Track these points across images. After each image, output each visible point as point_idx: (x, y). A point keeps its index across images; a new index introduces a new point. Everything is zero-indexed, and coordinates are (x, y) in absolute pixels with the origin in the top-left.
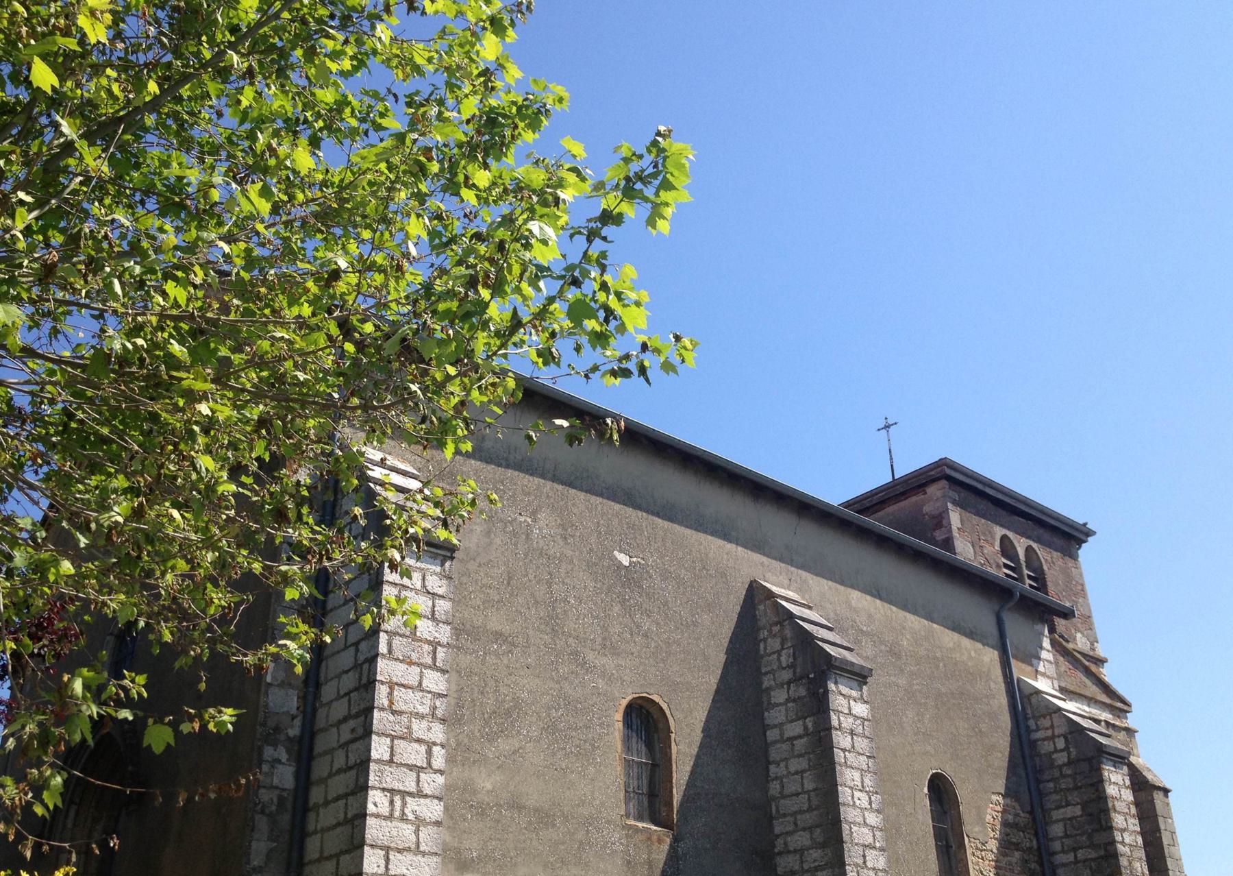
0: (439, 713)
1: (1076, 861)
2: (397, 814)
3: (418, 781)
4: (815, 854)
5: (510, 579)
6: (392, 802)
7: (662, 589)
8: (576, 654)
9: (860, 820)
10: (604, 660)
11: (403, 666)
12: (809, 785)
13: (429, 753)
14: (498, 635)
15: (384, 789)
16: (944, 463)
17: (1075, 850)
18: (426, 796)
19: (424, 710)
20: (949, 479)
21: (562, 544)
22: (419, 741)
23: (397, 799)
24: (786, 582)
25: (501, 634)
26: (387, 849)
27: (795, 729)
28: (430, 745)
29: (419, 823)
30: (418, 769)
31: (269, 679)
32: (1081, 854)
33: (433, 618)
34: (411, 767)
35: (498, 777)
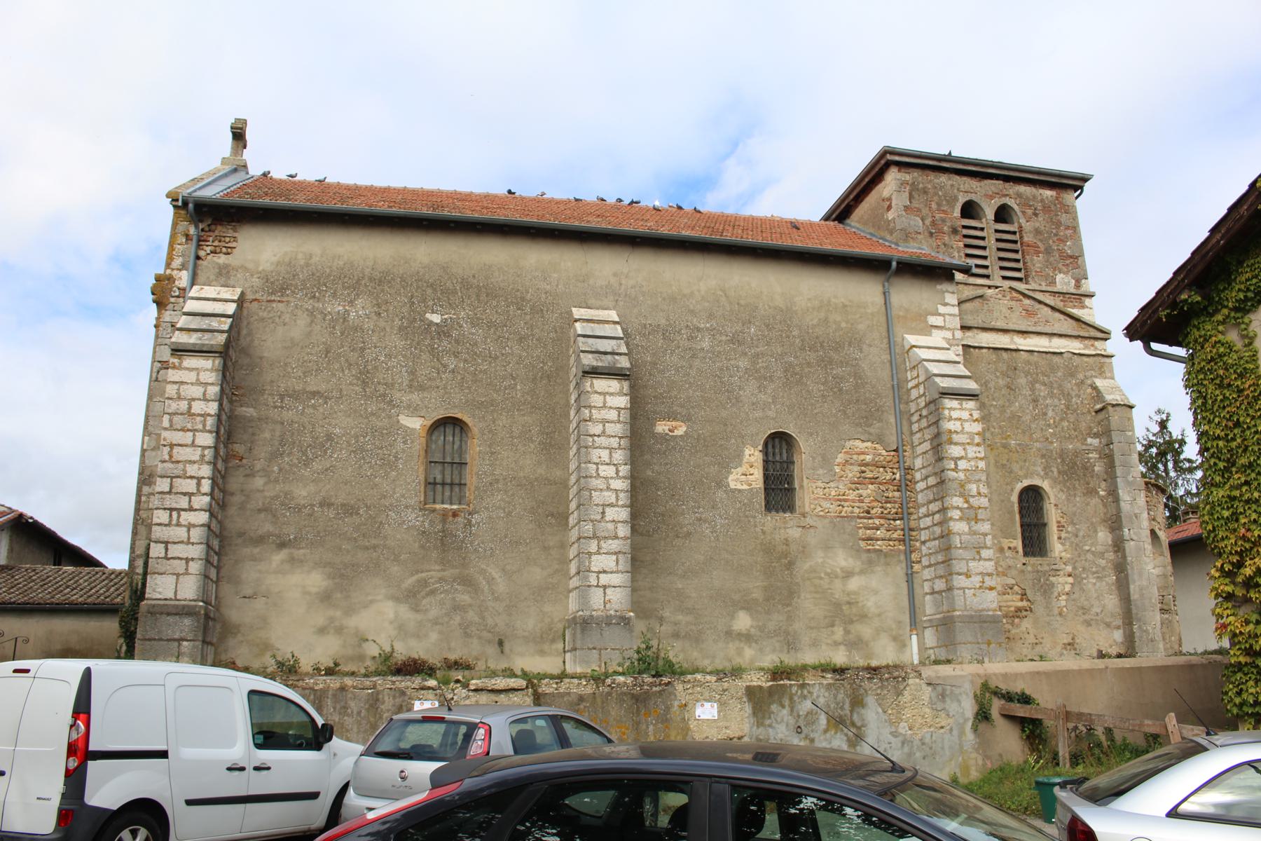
0: (207, 459)
2: (174, 522)
5: (328, 352)
13: (199, 484)
14: (315, 394)
16: (886, 152)
17: (926, 478)
19: (197, 458)
22: (191, 477)
23: (175, 514)
24: (611, 304)
25: (318, 392)
26: (166, 543)
28: (199, 479)
29: (190, 526)
30: (190, 495)
34: (185, 494)
35: (312, 488)
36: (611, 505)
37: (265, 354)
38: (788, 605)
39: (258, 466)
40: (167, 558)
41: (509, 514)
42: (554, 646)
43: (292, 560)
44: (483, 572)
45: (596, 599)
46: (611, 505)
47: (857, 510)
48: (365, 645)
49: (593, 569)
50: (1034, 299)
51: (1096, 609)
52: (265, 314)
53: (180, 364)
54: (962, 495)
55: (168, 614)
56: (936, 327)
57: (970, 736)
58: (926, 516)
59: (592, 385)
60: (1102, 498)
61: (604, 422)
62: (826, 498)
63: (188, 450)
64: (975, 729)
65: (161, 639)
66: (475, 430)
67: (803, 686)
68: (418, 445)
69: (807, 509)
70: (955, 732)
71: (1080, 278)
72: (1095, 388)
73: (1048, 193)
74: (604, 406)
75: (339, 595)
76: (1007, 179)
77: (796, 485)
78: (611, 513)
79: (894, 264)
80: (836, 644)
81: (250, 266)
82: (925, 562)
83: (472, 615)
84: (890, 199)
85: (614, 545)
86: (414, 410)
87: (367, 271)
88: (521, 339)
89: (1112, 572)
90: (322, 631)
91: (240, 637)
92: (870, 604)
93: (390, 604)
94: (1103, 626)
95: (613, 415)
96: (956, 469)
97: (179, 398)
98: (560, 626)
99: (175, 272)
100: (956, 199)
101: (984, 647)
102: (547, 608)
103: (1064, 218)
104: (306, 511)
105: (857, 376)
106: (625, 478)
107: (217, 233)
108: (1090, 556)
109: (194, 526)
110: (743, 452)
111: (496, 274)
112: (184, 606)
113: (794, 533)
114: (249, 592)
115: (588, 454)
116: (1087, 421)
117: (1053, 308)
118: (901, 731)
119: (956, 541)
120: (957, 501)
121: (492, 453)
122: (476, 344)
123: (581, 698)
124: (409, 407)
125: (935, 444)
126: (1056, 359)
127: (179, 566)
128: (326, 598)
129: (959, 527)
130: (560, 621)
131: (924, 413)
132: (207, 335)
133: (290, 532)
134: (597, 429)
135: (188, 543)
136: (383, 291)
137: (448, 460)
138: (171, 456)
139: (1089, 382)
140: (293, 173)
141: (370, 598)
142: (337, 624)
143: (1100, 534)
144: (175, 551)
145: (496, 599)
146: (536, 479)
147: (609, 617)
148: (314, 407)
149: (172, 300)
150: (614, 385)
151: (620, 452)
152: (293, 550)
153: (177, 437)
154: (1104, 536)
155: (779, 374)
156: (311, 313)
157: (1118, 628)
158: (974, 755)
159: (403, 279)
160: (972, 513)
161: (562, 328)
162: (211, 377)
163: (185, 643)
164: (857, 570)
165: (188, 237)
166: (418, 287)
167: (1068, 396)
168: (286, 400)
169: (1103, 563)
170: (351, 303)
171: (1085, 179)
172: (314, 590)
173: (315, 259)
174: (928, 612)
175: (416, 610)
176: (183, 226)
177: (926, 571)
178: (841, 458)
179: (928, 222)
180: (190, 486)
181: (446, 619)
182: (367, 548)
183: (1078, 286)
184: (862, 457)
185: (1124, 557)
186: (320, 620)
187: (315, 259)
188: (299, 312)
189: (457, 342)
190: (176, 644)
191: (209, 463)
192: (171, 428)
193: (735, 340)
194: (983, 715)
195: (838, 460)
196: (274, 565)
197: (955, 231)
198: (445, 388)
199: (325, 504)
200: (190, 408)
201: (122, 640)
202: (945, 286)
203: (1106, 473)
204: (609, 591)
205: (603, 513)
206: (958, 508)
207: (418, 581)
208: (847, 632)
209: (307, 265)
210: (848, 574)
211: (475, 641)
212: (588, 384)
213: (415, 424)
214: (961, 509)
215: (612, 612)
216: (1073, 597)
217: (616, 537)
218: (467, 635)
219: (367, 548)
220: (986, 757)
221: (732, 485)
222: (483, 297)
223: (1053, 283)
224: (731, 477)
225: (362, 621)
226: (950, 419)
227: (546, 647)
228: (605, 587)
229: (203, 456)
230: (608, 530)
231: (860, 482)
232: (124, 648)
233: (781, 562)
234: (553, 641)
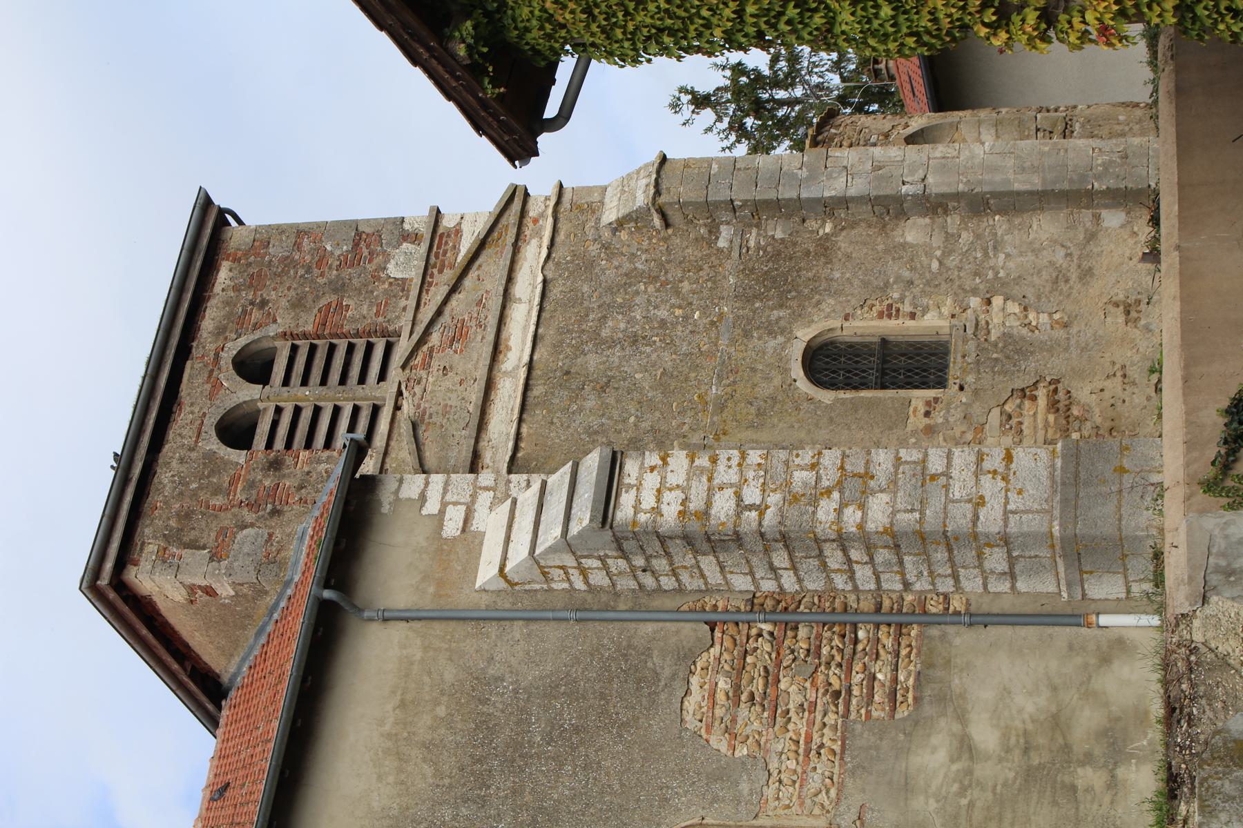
16: (92, 587)
17: (773, 569)
20: (122, 562)
47: (831, 719)
54: (814, 502)
56: (467, 521)
62: (801, 780)
71: (399, 231)
72: (620, 224)
73: (224, 275)
76: (184, 353)
79: (327, 594)
80: (1113, 784)
89: (986, 223)
92: (1029, 705)
96: (761, 509)
100: (210, 456)
101: (1127, 480)
103: (277, 251)
108: (953, 261)
116: (684, 246)
117: (454, 289)
119: (907, 519)
120: (826, 511)
126: (555, 292)
129: (878, 512)
131: (639, 561)
139: (607, 234)
143: (909, 239)
154: (914, 232)
157: (1097, 218)
160: (850, 484)
164: (956, 727)
167: (631, 276)
169: (966, 237)
171: (205, 203)
174: (1052, 588)
178: (719, 743)
179: (249, 516)
183: (415, 238)
184: (720, 697)
185: (957, 196)
195: (724, 748)
203: (789, 217)
206: (839, 512)
210: (965, 747)
216: (1031, 298)
223: (403, 284)
226: (657, 511)
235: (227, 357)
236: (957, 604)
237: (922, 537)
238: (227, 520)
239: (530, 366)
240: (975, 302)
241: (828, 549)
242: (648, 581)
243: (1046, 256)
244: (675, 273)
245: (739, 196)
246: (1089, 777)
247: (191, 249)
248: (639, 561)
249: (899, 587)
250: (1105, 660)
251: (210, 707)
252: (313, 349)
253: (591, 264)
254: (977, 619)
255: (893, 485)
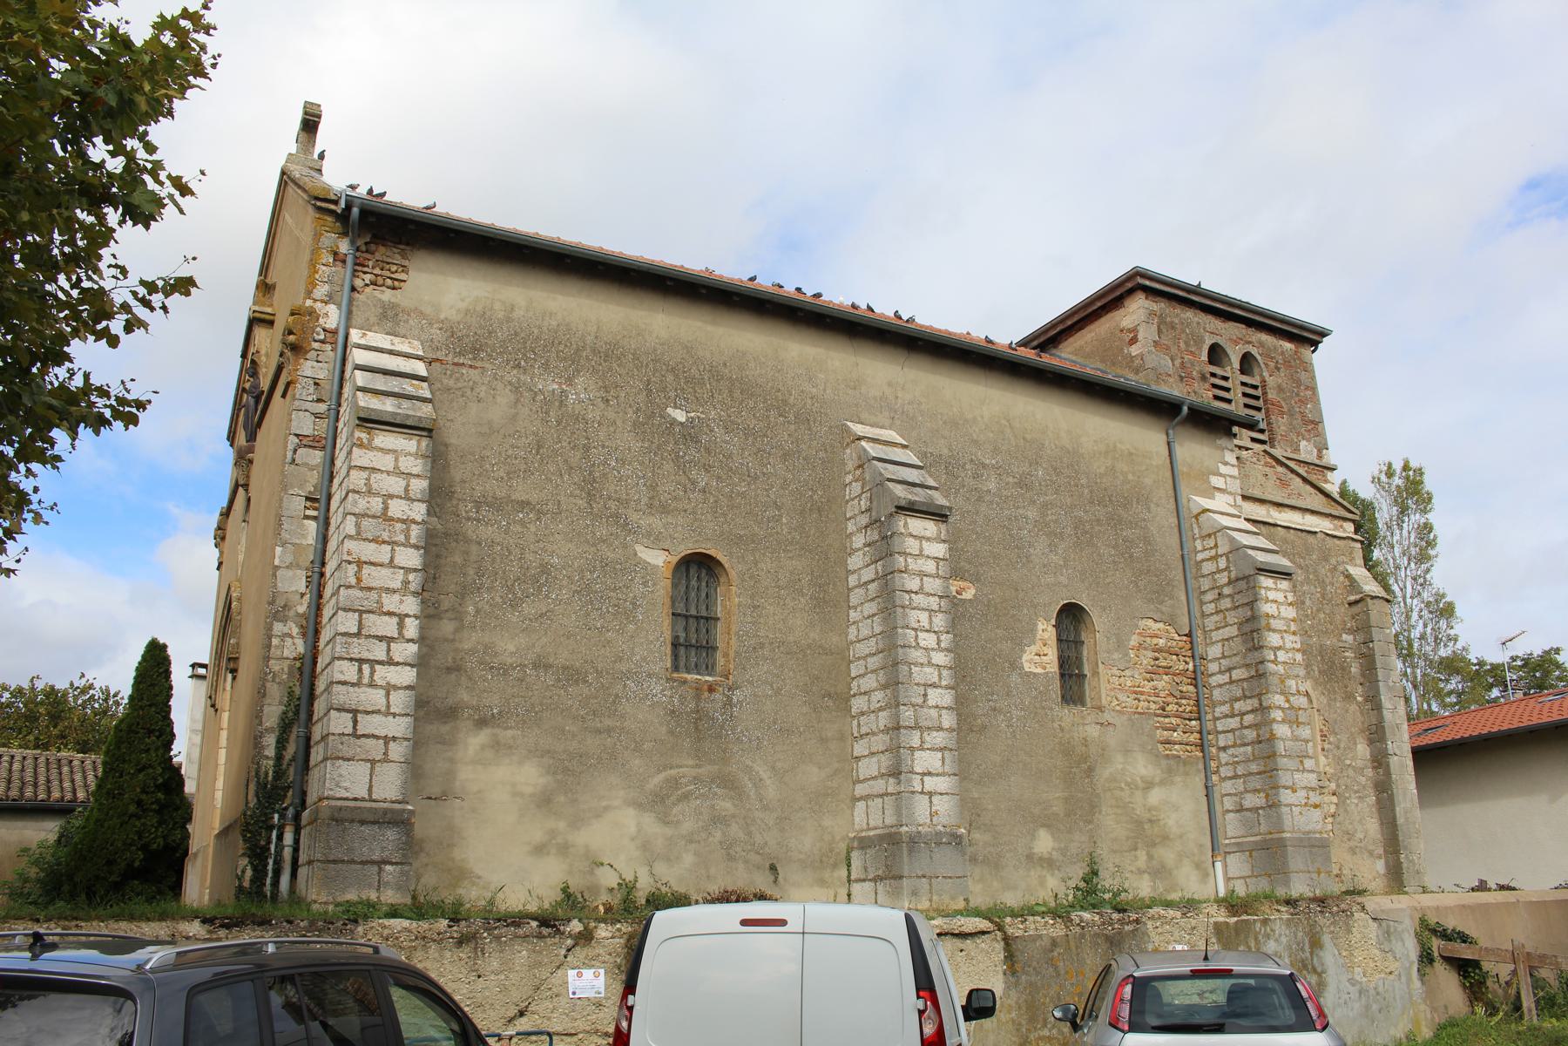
0: (413, 587)
1: (1231, 682)
2: (366, 680)
3: (389, 650)
4: (879, 695)
5: (539, 447)
6: (360, 670)
7: (726, 442)
8: (617, 516)
9: (924, 660)
10: (651, 520)
11: (373, 545)
12: (878, 629)
13: (401, 625)
14: (524, 505)
15: (351, 659)
16: (1137, 273)
17: (1229, 670)
18: (398, 664)
19: (397, 584)
20: (1145, 289)
21: (602, 406)
22: (390, 614)
23: (366, 668)
24: (887, 422)
25: (528, 503)
26: (355, 712)
27: (868, 574)
28: (402, 618)
29: (389, 688)
30: (389, 640)
31: (277, 562)
32: (1236, 674)
33: (408, 498)
34: (381, 638)
36: (934, 686)
37: (453, 441)
38: (1090, 822)
39: (446, 605)
40: (355, 735)
41: (778, 692)
42: (835, 874)
43: (496, 745)
44: (748, 770)
45: (921, 809)
46: (934, 686)
47: (1153, 706)
48: (600, 871)
49: (918, 769)
50: (1287, 467)
51: (1360, 835)
52: (451, 383)
53: (370, 440)
54: (1282, 693)
55: (362, 822)
56: (1219, 489)
57: (1417, 984)
58: (1226, 716)
59: (906, 524)
60: (1358, 703)
61: (922, 575)
62: (1121, 688)
63: (385, 572)
64: (1422, 975)
65: (352, 862)
66: (733, 574)
67: (1265, 922)
68: (662, 588)
69: (1104, 702)
70: (1403, 979)
71: (1322, 447)
72: (1348, 576)
73: (1288, 346)
74: (921, 555)
75: (562, 799)
76: (1249, 323)
77: (1087, 671)
78: (935, 696)
79: (1185, 409)
80: (1141, 872)
81: (428, 310)
82: (1225, 771)
83: (735, 830)
84: (1134, 330)
85: (938, 738)
86: (655, 540)
87: (589, 339)
88: (786, 456)
89: (1371, 791)
90: (539, 850)
91: (423, 859)
92: (1171, 821)
93: (631, 812)
94: (1366, 855)
95: (930, 567)
96: (1275, 662)
97: (370, 492)
98: (843, 846)
99: (318, 305)
100: (1201, 341)
101: (1315, 876)
102: (827, 822)
103: (1303, 376)
104: (515, 674)
105: (1147, 540)
106: (947, 650)
107: (378, 256)
108: (1351, 772)
109: (396, 688)
110: (1035, 625)
111: (752, 365)
112: (385, 811)
113: (1093, 731)
114: (435, 791)
115: (905, 616)
116: (1343, 613)
117: (1305, 480)
118: (1358, 978)
119: (1280, 747)
120: (1279, 700)
121: (755, 607)
122: (730, 456)
123: (1054, 943)
124: (649, 534)
125: (1247, 628)
126: (1311, 538)
127: (375, 748)
128: (544, 801)
129: (1282, 730)
130: (843, 839)
131: (1226, 591)
132: (406, 404)
133: (493, 702)
134: (913, 584)
135: (388, 713)
136: (610, 369)
137: (693, 612)
138: (359, 580)
139: (1341, 568)
140: (354, 182)
141: (604, 804)
142: (560, 840)
143: (1359, 746)
144: (367, 724)
145: (765, 808)
146: (809, 646)
147: (938, 834)
148: (522, 523)
149: (316, 345)
150: (926, 527)
151: (940, 616)
152: (497, 731)
153: (368, 551)
154: (1363, 750)
155: (1069, 530)
156: (516, 389)
157: (1379, 857)
158: (1423, 1007)
159: (636, 358)
160: (1293, 713)
161: (832, 446)
162: (415, 466)
163: (388, 868)
164: (1157, 780)
165: (338, 258)
166: (656, 370)
167: (1323, 584)
168: (484, 510)
169: (1363, 780)
170: (570, 381)
171: (1323, 334)
172: (529, 790)
173: (518, 313)
174: (1230, 834)
175: (665, 820)
176: (329, 239)
177: (1229, 783)
178: (1134, 640)
179: (1178, 362)
180: (388, 626)
181: (704, 835)
182: (598, 731)
183: (1320, 457)
184: (1155, 641)
185: (1388, 773)
186: (538, 836)
187: (518, 313)
188: (500, 386)
189: (708, 451)
190: (376, 868)
191: (415, 594)
192: (358, 536)
193: (1023, 483)
194: (1426, 958)
195: (1132, 643)
196: (471, 751)
197: (1203, 378)
198: (694, 513)
199: (541, 665)
200: (386, 508)
201: (245, 861)
202: (1223, 442)
203: (1363, 675)
204: (935, 799)
205: (925, 695)
206: (1279, 707)
207: (667, 780)
208: (1150, 857)
209: (509, 320)
210: (1149, 785)
211: (741, 866)
212: (901, 523)
213: (658, 559)
214: (1282, 709)
215: (940, 828)
216: (1338, 819)
217: (940, 729)
218: (730, 858)
219: (598, 731)
220: (1434, 1009)
221: (1027, 667)
222: (737, 394)
223: (1297, 450)
224: (1025, 657)
225: (594, 836)
226: (1267, 600)
227: (827, 875)
228: (931, 794)
229: (406, 583)
230: (931, 719)
231: (1153, 673)
232: (249, 873)
233: (1080, 766)
234: (835, 866)
235: (1250, 348)
236: (1215, 778)
237: (1272, 755)
238: (1174, 350)
239: (1275, 525)
240: (1333, 786)
241: (1255, 702)
242: (1209, 596)
243: (1359, 828)
244: (1327, 609)
245: (1376, 646)
246: (1142, 855)
247: (1302, 326)
248: (1226, 591)
249: (1222, 744)
250: (1198, 866)
251: (1035, 343)
252: (1257, 398)
253: (1326, 560)
254: (1208, 790)
255: (1296, 739)
